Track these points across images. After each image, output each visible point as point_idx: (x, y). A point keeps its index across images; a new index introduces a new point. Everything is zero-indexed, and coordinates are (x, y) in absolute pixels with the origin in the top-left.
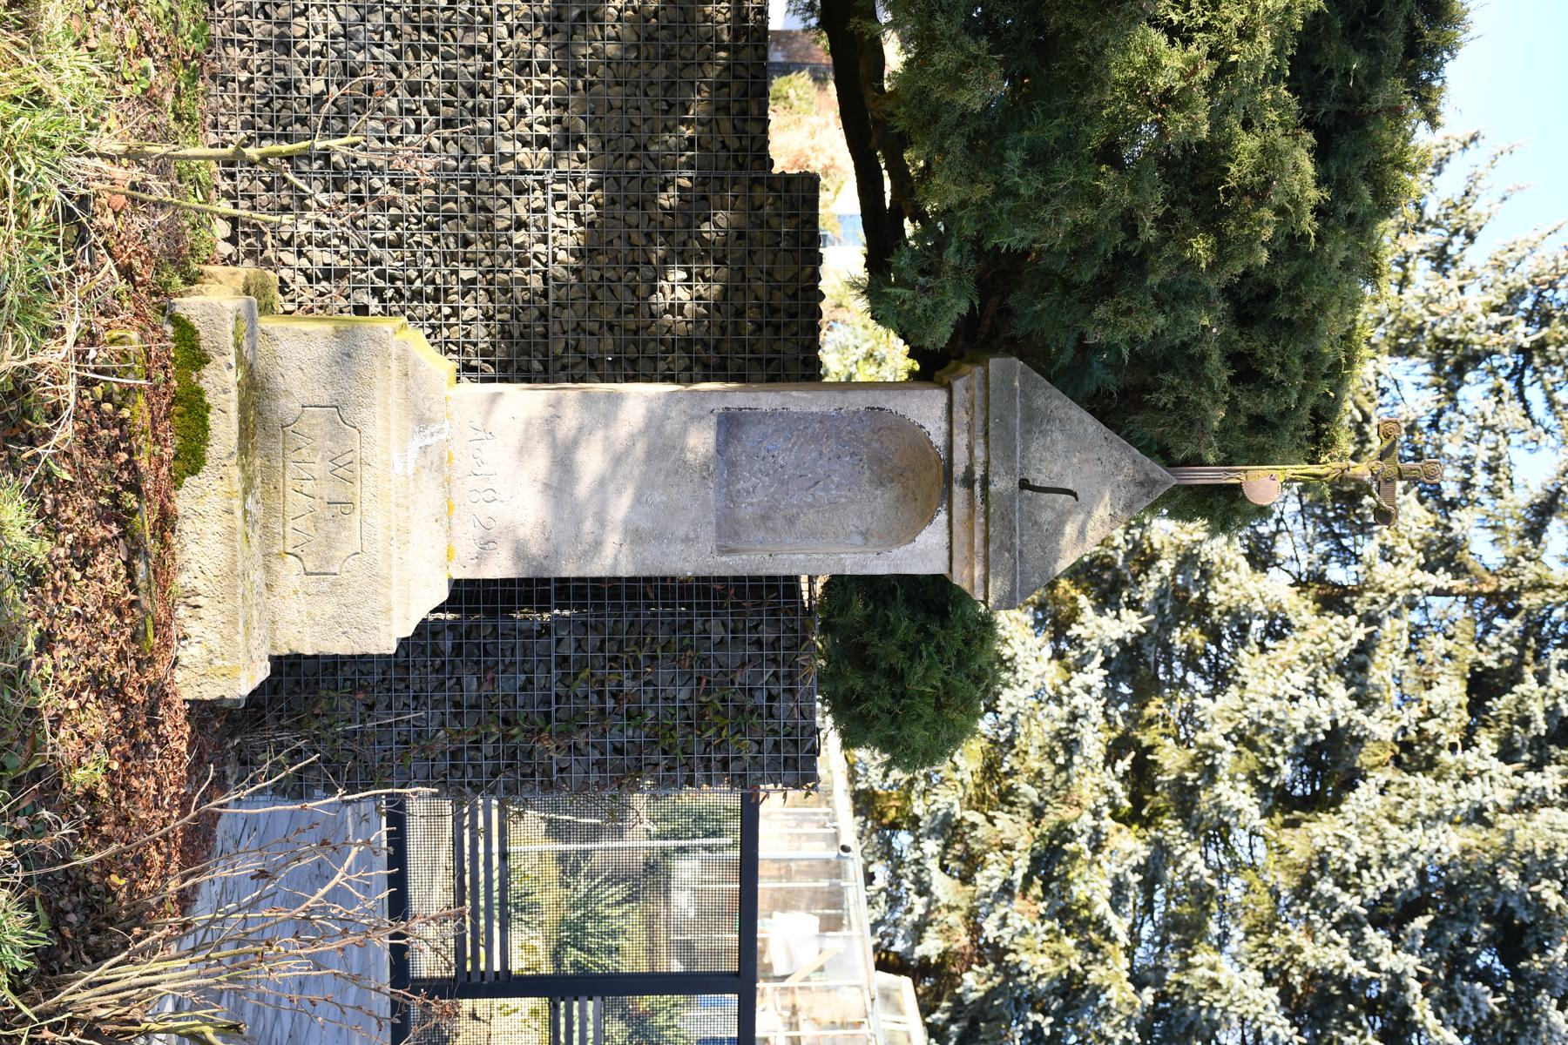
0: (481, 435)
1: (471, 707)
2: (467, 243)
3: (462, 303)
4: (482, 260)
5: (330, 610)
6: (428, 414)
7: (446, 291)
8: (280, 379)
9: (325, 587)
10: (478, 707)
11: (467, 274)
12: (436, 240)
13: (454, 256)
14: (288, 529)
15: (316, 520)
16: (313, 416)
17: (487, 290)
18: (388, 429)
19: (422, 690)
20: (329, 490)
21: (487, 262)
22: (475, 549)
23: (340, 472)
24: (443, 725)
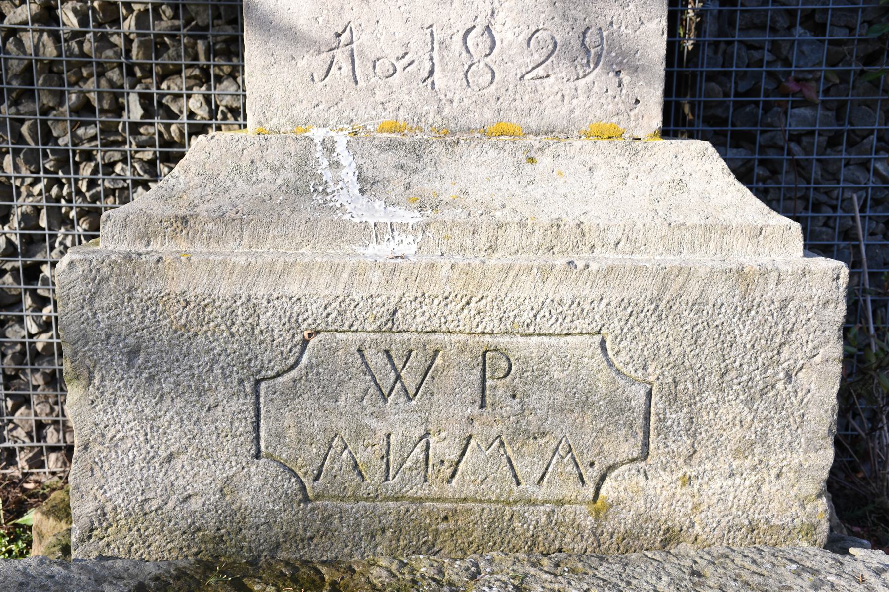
0: (341, 56)
1: (839, 118)
2: (85, 108)
3: (184, 119)
4: (111, 83)
5: (733, 407)
6: (288, 174)
7: (165, 143)
8: (196, 504)
9: (677, 418)
10: (842, 105)
11: (136, 112)
12: (88, 156)
13: (108, 129)
14: (541, 494)
15: (522, 434)
16: (279, 436)
17: (162, 79)
18: (308, 267)
19: (805, 198)
20: (451, 409)
21: (113, 75)
22: (599, 78)
23: (410, 379)
24: (865, 165)
